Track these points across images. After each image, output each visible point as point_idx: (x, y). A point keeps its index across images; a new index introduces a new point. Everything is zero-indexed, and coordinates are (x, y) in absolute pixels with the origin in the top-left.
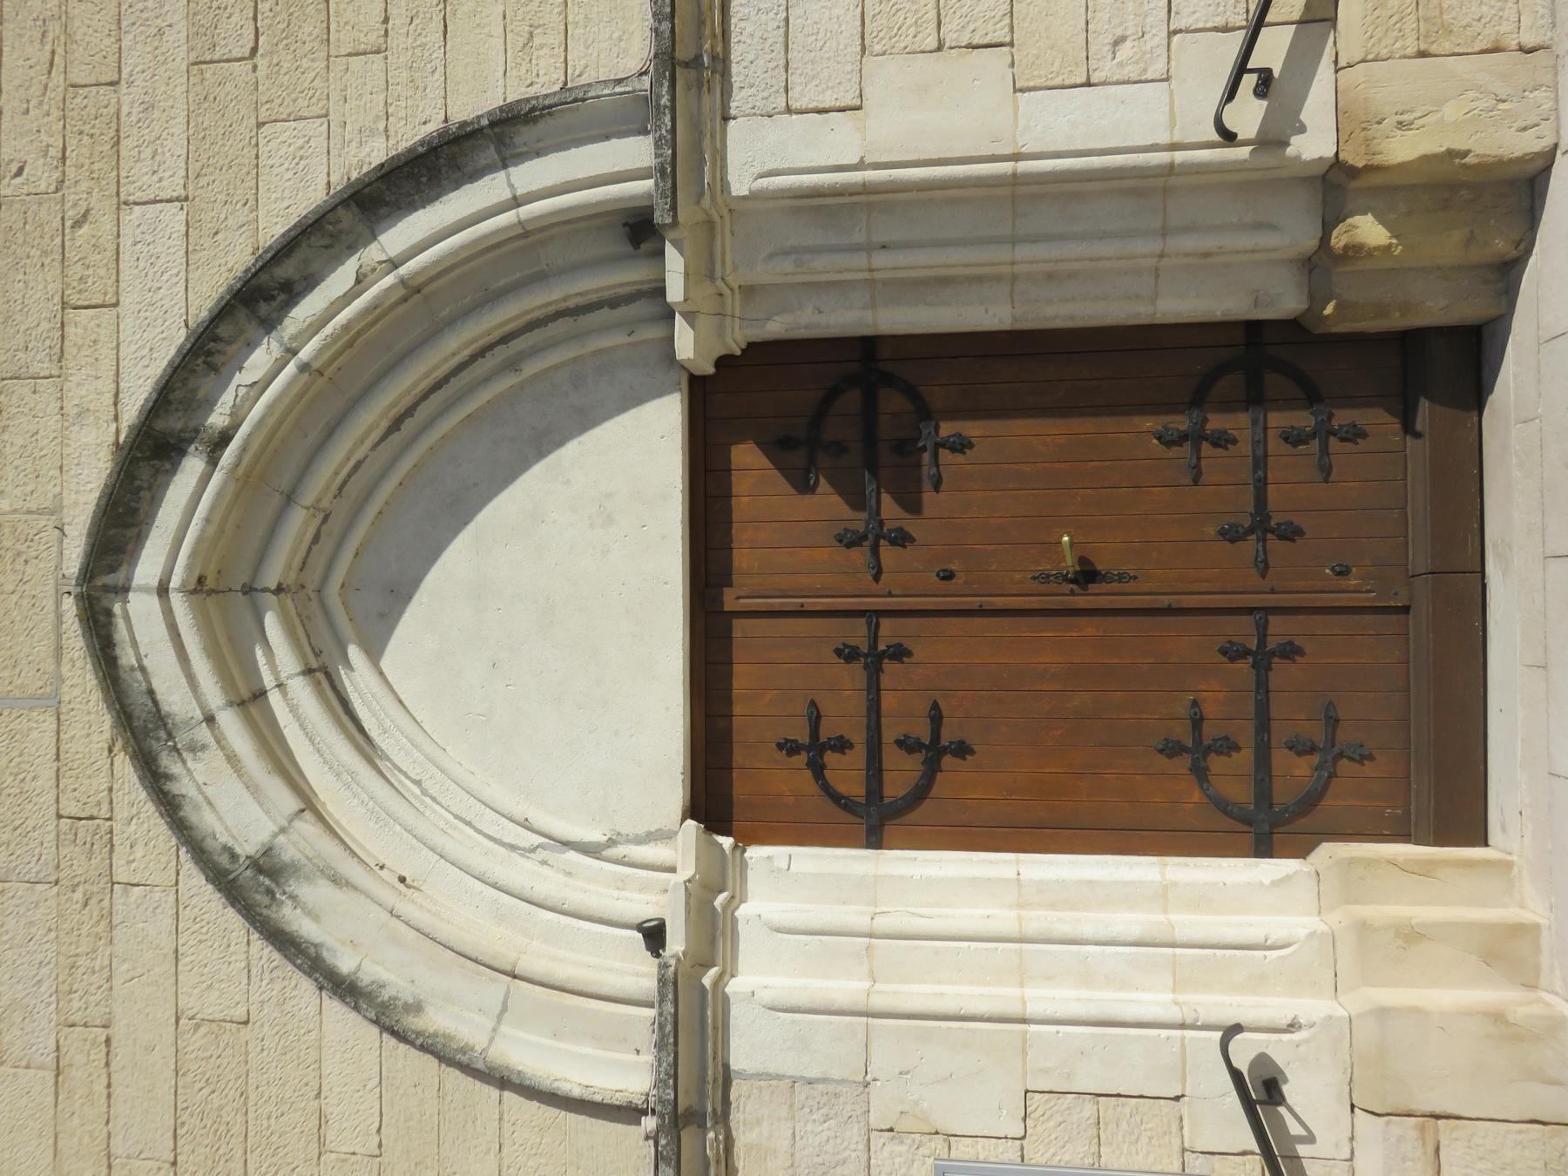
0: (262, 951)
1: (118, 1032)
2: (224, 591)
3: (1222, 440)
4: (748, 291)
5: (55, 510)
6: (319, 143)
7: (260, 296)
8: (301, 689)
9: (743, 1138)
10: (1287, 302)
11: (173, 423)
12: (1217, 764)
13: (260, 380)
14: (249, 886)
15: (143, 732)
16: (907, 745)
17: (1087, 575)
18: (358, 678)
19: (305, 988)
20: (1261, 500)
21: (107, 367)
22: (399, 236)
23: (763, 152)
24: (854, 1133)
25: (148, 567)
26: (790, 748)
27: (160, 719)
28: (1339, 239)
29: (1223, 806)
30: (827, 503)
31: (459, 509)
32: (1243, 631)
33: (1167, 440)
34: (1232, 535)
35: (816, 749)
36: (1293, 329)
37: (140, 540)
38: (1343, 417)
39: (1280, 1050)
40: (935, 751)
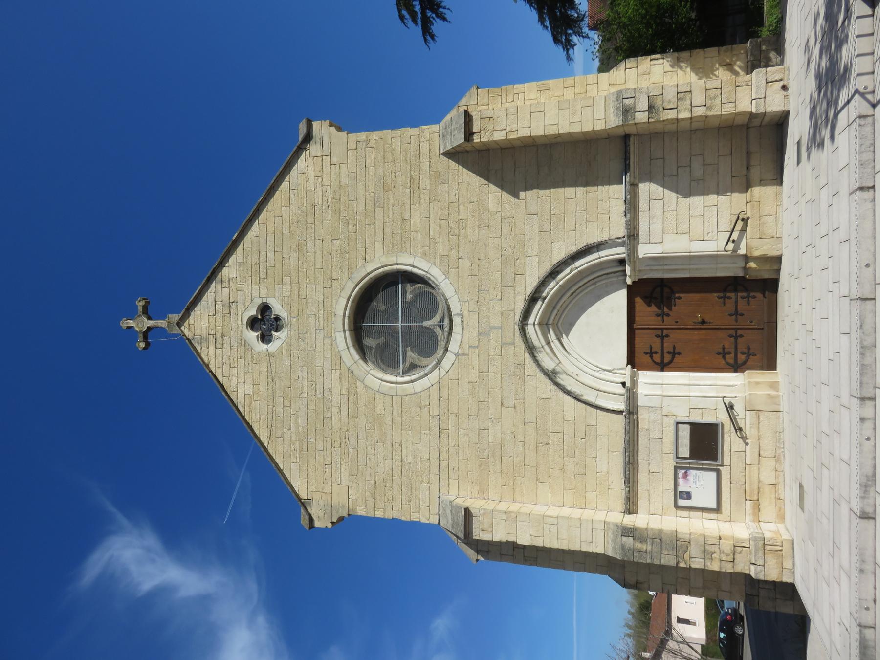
0: (554, 387)
1: (526, 401)
2: (544, 325)
3: (729, 298)
4: (640, 271)
5: (513, 310)
6: (563, 247)
7: (553, 274)
8: (557, 342)
9: (640, 417)
10: (740, 274)
11: (537, 295)
12: (727, 356)
13: (552, 288)
14: (551, 376)
15: (531, 349)
16: (669, 353)
17: (703, 322)
18: (565, 340)
19: (561, 394)
20: (736, 309)
21: (523, 285)
22: (578, 263)
23: (644, 250)
24: (660, 416)
25: (531, 320)
26: (646, 353)
27: (534, 347)
28: (748, 266)
29: (728, 363)
30: (654, 308)
31: (583, 309)
32: (732, 332)
33: (719, 298)
34: (731, 315)
35: (651, 353)
36: (743, 278)
37: (530, 316)
38: (752, 294)
39: (733, 401)
40: (674, 354)
